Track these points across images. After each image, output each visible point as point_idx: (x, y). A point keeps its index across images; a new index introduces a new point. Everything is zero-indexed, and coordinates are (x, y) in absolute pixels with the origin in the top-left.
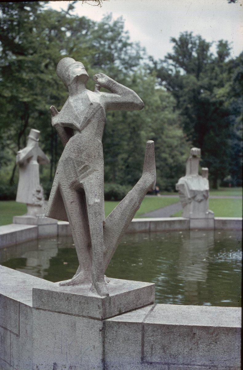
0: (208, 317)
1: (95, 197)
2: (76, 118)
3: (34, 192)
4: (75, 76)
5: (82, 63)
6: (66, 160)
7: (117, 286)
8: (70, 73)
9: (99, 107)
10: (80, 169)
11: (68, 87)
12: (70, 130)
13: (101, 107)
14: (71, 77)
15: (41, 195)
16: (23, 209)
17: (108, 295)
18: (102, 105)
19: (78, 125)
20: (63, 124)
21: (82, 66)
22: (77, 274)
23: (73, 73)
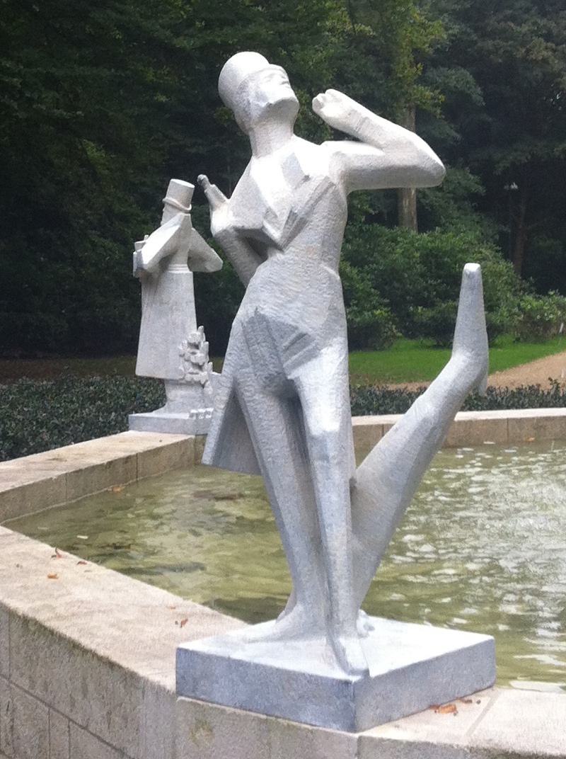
0: (545, 507)
1: (326, 411)
2: (268, 213)
3: (183, 348)
4: (263, 105)
5: (280, 68)
6: (251, 321)
7: (388, 646)
8: (249, 98)
9: (327, 185)
10: (286, 344)
11: (214, 510)
12: (257, 244)
13: (332, 185)
14: (252, 107)
15: (201, 355)
16: (152, 394)
17: (367, 672)
18: (336, 181)
19: (275, 233)
20: (237, 230)
21: (283, 77)
22: (289, 609)
23: (260, 97)
